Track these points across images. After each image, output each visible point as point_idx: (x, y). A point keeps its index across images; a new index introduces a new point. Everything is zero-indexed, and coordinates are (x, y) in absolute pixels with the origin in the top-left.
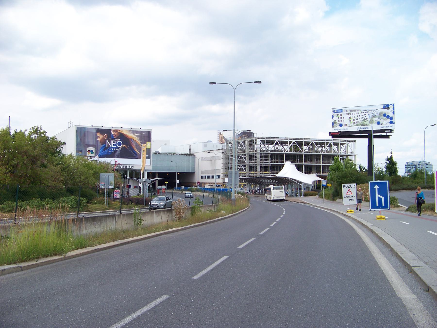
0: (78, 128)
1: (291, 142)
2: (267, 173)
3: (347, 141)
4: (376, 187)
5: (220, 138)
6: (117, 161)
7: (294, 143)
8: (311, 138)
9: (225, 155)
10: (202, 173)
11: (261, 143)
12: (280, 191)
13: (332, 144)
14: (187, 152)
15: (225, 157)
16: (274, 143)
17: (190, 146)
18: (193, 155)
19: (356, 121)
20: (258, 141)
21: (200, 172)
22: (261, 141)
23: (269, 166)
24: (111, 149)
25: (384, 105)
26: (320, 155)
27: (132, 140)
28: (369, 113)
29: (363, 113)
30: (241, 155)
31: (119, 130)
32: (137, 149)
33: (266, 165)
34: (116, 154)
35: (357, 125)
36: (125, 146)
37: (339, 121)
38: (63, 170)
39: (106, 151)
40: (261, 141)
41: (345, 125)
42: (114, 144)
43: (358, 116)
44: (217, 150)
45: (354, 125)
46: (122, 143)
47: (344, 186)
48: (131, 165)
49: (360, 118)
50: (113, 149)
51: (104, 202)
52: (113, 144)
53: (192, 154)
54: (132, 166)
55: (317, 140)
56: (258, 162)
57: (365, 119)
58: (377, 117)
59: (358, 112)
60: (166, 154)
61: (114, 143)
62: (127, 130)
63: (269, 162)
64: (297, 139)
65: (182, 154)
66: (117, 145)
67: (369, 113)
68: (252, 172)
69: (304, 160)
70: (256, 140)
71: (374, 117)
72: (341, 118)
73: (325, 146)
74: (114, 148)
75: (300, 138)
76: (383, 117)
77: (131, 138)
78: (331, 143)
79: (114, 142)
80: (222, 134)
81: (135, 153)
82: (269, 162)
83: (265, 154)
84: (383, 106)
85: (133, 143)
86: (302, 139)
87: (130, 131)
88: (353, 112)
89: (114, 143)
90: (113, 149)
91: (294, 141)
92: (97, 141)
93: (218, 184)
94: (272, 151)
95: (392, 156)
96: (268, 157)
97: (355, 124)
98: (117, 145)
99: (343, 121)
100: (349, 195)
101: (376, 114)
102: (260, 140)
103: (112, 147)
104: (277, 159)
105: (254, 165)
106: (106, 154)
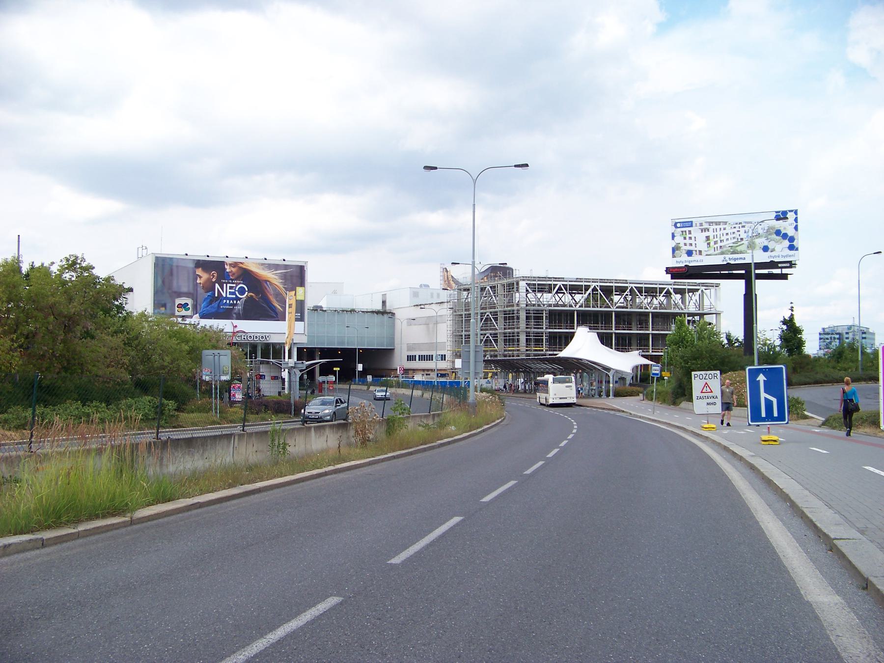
0: (157, 258)
1: (589, 286)
2: (539, 350)
3: (702, 286)
4: (761, 378)
5: (446, 278)
6: (236, 326)
7: (595, 289)
8: (629, 278)
9: (455, 314)
10: (408, 350)
11: (528, 288)
12: (567, 387)
13: (672, 291)
14: (378, 307)
15: (455, 317)
16: (554, 290)
17: (384, 295)
18: (390, 313)
19: (719, 244)
20: (522, 284)
21: (405, 347)
22: (528, 285)
23: (544, 335)
24: (225, 301)
25: (777, 212)
26: (647, 314)
27: (268, 283)
28: (746, 229)
29: (735, 227)
30: (487, 314)
31: (241, 263)
32: (277, 300)
33: (539, 333)
34: (235, 311)
35: (722, 253)
36: (253, 294)
37: (685, 245)
38: (127, 343)
39: (215, 305)
40: (528, 285)
41: (698, 252)
42: (231, 291)
43: (725, 235)
44: (439, 303)
45: (716, 252)
46: (247, 290)
47: (696, 376)
48: (265, 334)
49: (727, 239)
50: (228, 301)
51: (211, 409)
52: (229, 290)
53: (389, 311)
54: (267, 335)
55: (642, 283)
56: (522, 328)
57: (739, 240)
58: (762, 236)
59: (725, 226)
60: (336, 311)
61: (230, 289)
62: (256, 263)
63: (544, 328)
64: (602, 281)
65: (369, 312)
66: (237, 292)
67: (746, 229)
68: (510, 349)
69: (616, 324)
70: (518, 284)
71: (756, 236)
72: (690, 238)
73: (658, 294)
74: (230, 299)
75: (607, 280)
76: (774, 236)
77: (264, 279)
78: (670, 289)
79: (231, 288)
80: (448, 270)
81: (273, 309)
82: (544, 328)
83: (536, 311)
84: (775, 214)
85: (268, 289)
86: (610, 281)
87: (263, 264)
88: (715, 227)
89: (230, 289)
90: (228, 301)
91: (594, 284)
92: (196, 285)
93: (441, 373)
94: (550, 305)
95: (792, 315)
96: (542, 318)
97: (719, 251)
98: (237, 292)
99: (693, 245)
100: (706, 395)
101: (760, 231)
102: (526, 284)
103: (226, 298)
104: (560, 322)
105: (513, 333)
106: (214, 310)
